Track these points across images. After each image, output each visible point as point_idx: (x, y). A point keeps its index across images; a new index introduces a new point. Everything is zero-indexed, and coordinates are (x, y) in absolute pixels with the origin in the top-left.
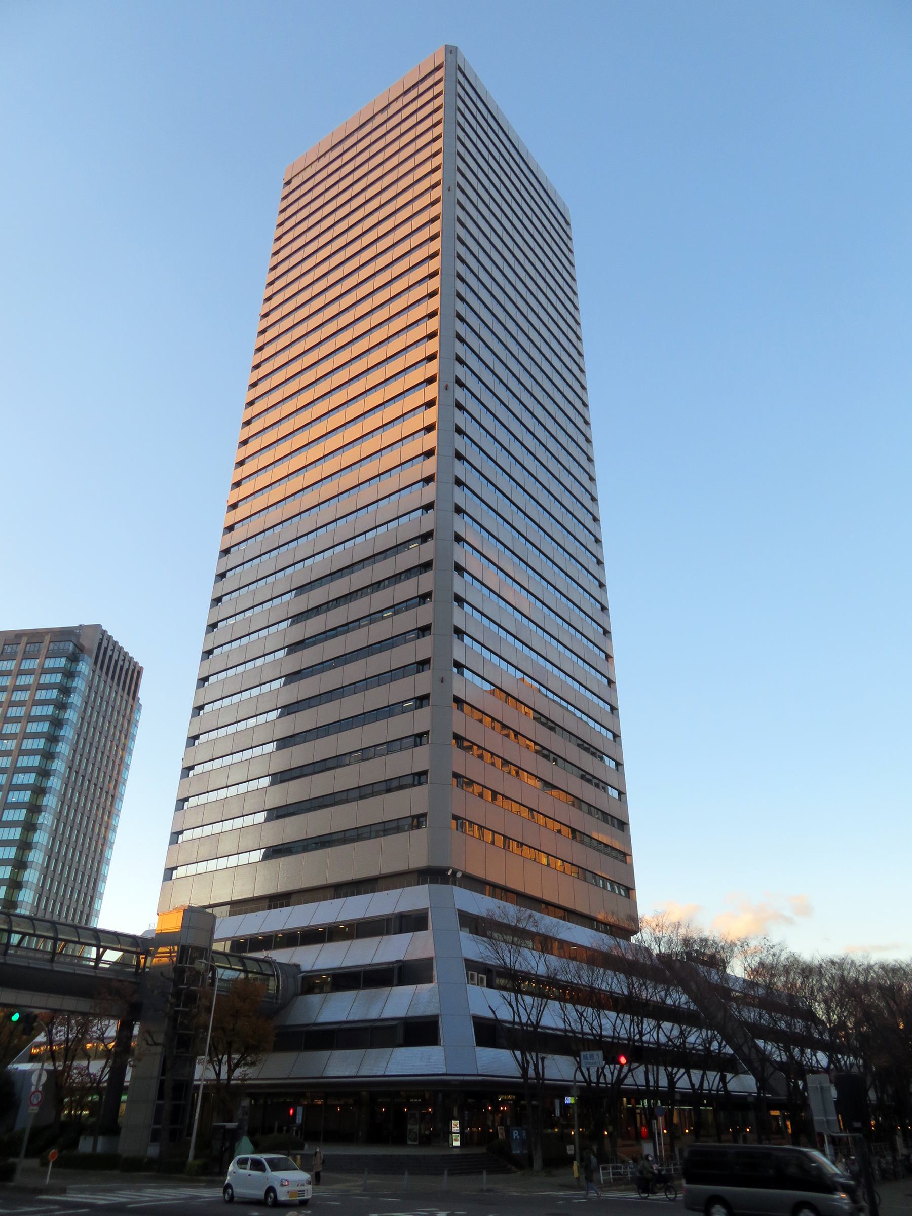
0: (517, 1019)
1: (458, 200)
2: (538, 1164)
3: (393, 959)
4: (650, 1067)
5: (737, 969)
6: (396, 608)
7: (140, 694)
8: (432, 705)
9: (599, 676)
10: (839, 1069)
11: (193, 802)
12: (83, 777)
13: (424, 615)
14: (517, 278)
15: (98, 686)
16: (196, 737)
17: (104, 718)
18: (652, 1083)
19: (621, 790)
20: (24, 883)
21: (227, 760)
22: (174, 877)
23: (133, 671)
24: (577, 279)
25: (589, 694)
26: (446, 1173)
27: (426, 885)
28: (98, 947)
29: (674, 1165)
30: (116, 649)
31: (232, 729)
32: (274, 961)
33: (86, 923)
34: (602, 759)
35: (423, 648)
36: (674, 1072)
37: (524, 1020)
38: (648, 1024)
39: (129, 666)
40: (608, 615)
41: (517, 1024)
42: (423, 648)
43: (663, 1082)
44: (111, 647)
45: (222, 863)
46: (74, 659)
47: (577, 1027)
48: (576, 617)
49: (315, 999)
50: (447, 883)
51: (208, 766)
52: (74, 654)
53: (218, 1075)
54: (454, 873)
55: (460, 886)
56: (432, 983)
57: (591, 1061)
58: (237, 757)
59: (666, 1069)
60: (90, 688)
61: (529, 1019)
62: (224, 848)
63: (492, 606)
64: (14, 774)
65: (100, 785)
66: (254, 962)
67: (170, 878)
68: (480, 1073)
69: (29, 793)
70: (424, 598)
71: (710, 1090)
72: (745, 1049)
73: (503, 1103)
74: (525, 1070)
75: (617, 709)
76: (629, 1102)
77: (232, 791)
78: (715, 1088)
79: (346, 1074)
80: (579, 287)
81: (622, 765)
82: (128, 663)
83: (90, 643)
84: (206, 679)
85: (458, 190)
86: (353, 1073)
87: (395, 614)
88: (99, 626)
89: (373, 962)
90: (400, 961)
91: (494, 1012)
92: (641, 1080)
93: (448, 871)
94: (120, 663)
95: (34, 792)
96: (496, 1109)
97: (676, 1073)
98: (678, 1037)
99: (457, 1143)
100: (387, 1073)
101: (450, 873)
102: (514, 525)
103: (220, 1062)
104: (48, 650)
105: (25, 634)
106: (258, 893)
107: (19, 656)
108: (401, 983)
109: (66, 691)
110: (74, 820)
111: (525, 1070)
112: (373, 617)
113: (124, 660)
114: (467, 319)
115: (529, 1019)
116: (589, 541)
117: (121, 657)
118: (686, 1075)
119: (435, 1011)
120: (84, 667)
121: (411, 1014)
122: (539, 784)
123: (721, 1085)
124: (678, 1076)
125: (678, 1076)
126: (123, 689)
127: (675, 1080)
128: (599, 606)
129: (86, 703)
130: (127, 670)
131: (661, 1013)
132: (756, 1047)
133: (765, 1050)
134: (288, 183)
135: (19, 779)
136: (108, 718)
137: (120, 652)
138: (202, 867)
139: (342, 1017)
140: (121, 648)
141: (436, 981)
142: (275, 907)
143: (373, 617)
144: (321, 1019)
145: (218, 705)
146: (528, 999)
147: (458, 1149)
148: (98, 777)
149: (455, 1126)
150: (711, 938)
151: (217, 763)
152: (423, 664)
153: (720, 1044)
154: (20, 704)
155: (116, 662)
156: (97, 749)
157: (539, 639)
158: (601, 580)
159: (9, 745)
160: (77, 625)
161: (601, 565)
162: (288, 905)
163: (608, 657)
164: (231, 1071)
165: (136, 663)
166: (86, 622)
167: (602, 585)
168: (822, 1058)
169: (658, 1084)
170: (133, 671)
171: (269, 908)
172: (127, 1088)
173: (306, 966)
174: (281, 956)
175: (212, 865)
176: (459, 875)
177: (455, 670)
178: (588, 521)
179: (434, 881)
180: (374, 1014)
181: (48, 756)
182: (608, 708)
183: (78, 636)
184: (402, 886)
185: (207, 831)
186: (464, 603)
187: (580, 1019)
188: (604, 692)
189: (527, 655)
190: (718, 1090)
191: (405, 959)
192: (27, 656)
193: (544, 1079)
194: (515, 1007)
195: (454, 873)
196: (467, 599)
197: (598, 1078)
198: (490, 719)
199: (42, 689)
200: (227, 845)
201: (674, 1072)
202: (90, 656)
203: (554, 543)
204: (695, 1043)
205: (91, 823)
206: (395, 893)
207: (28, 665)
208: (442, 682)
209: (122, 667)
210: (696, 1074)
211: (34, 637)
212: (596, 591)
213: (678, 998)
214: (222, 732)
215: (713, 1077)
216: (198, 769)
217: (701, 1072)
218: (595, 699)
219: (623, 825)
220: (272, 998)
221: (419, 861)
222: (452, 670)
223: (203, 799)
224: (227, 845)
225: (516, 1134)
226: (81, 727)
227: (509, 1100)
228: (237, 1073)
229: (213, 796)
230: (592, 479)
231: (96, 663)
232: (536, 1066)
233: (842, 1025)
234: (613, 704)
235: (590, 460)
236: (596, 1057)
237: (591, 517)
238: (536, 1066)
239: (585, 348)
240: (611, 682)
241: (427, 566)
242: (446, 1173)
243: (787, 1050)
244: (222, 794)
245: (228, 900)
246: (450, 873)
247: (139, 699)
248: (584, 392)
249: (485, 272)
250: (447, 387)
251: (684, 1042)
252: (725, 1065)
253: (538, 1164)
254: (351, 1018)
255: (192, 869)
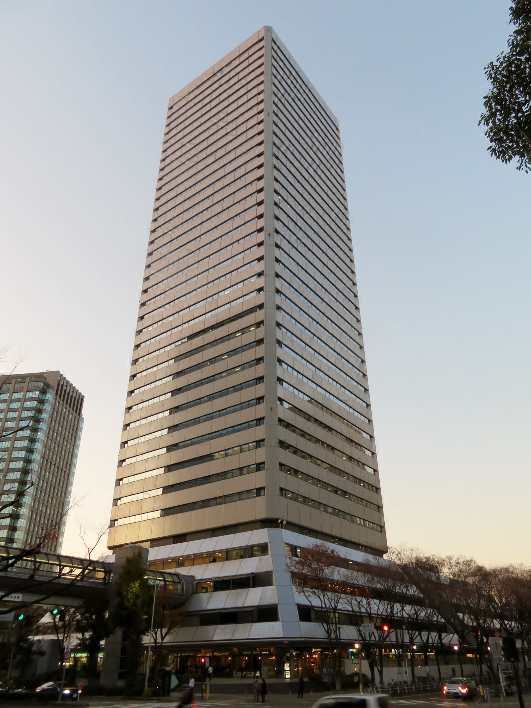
0: (324, 606)
1: (274, 121)
2: (338, 687)
3: (249, 572)
4: (398, 631)
5: (446, 572)
6: (243, 366)
7: (83, 412)
8: (266, 424)
9: (361, 402)
10: (506, 630)
11: (125, 481)
12: (51, 463)
13: (259, 370)
14: (300, 128)
15: (58, 408)
16: (126, 442)
17: (59, 424)
18: (400, 640)
19: (375, 469)
20: (18, 528)
21: (145, 456)
22: (116, 525)
23: (79, 398)
24: (340, 130)
25: (355, 413)
26: (290, 693)
27: (266, 530)
28: (60, 565)
29: (415, 686)
30: (74, 391)
31: (147, 438)
32: (180, 574)
33: (55, 551)
34: (360, 433)
35: (259, 390)
36: (413, 633)
37: (328, 605)
38: (397, 607)
39: (76, 395)
40: (364, 351)
41: (324, 608)
42: (259, 390)
43: (407, 639)
44: (65, 384)
45: (145, 517)
46: (43, 392)
47: (356, 609)
48: (347, 367)
49: (204, 596)
50: (277, 527)
51: (134, 460)
52: (43, 389)
53: (155, 641)
54: (282, 522)
55: (285, 529)
56: (272, 585)
57: (368, 629)
58: (151, 455)
59: (408, 632)
60: (54, 409)
61: (331, 604)
62: (145, 508)
63: (299, 364)
64: (10, 462)
65: (60, 467)
66: (168, 575)
67: (113, 526)
68: (303, 636)
69: (19, 473)
70: (259, 360)
71: (433, 643)
72: (452, 620)
73: (315, 653)
74: (329, 635)
75: (372, 421)
76: (385, 651)
77: (149, 474)
78: (436, 642)
79: (226, 638)
80: (353, 235)
81: (374, 437)
82: (75, 393)
83: (53, 383)
84: (130, 408)
85: (274, 115)
86: (230, 638)
87: (242, 369)
88: (58, 372)
89: (238, 574)
90: (253, 573)
91: (310, 602)
92: (394, 639)
93: (278, 520)
94: (71, 394)
95: (22, 473)
96: (311, 657)
97: (414, 634)
98: (414, 614)
99: (288, 676)
100: (249, 638)
101: (279, 521)
102: (310, 315)
103: (156, 633)
104: (28, 387)
105: (14, 377)
106: (166, 535)
107: (11, 391)
108: (255, 586)
109: (39, 411)
110: (46, 489)
111: (329, 635)
112: (230, 371)
113: (73, 392)
114: (280, 193)
115: (331, 604)
116: (353, 321)
117: (65, 384)
118: (419, 636)
119: (277, 602)
120: (50, 397)
121: (261, 604)
122: (188, 161)
123: (439, 641)
124: (415, 636)
125: (415, 636)
126: (73, 409)
127: (414, 638)
128: (358, 346)
129: (52, 418)
130: (75, 398)
131: (405, 600)
132: (458, 617)
133: (463, 620)
134: (171, 108)
135: (13, 465)
136: (61, 424)
137: (76, 393)
138: (132, 519)
139: (221, 606)
140: (77, 390)
141: (275, 584)
142: (177, 543)
143: (230, 371)
144: (209, 607)
145: (138, 423)
146: (329, 594)
147: (289, 680)
148: (59, 463)
149: (287, 667)
150: (500, 160)
151: (139, 458)
152: (260, 399)
153: (438, 617)
154: (12, 420)
155: (69, 393)
156: (69, 453)
157: (326, 382)
158: (358, 318)
159: (6, 444)
160: (45, 371)
161: (359, 322)
162: (185, 541)
163: (366, 390)
164: (163, 638)
165: (80, 393)
166: (51, 370)
167: (361, 347)
168: (497, 624)
169: (403, 640)
170: (79, 398)
171: (174, 543)
172: (103, 648)
173: (198, 577)
174: (183, 571)
175: (138, 518)
176: (285, 522)
177: (279, 402)
178: (354, 334)
179: (270, 526)
180: (240, 604)
181: (30, 451)
182: (366, 420)
183: (45, 378)
184: (252, 529)
185: (135, 498)
186: (283, 363)
187: (359, 605)
188: (364, 411)
189: (319, 392)
190: (437, 643)
191: (256, 572)
192: (15, 391)
193: (340, 639)
194: (322, 599)
195: (282, 522)
196: (285, 361)
197: (370, 637)
198: (299, 431)
199: (25, 411)
200: (147, 506)
201: (413, 633)
202: (53, 389)
203: (333, 324)
204: (424, 617)
205: (53, 488)
206: (248, 534)
207: (16, 396)
208: (271, 410)
209: (72, 396)
210: (424, 634)
211: (20, 379)
212: (358, 351)
213: (412, 591)
214: (142, 439)
215: (434, 635)
216: (128, 462)
217: (427, 633)
218: (359, 415)
219: (377, 489)
220: (180, 596)
221: (262, 515)
222: (277, 403)
223: (131, 479)
224: (147, 506)
225: (325, 670)
226: (49, 433)
227: (318, 651)
228: (167, 639)
229: (137, 478)
230: (353, 272)
231: (57, 394)
232: (335, 632)
233: (508, 603)
234: (364, 372)
235: (349, 239)
236: (370, 626)
237: (354, 307)
238: (335, 632)
239: (348, 196)
240: (368, 405)
241: (260, 342)
242: (290, 693)
243: (477, 620)
244: (143, 476)
245: (149, 538)
246: (279, 521)
247: (82, 415)
248: (349, 241)
249: (282, 133)
250: (269, 234)
251: (417, 616)
252: (441, 629)
253: (338, 687)
254: (226, 607)
255: (126, 521)
